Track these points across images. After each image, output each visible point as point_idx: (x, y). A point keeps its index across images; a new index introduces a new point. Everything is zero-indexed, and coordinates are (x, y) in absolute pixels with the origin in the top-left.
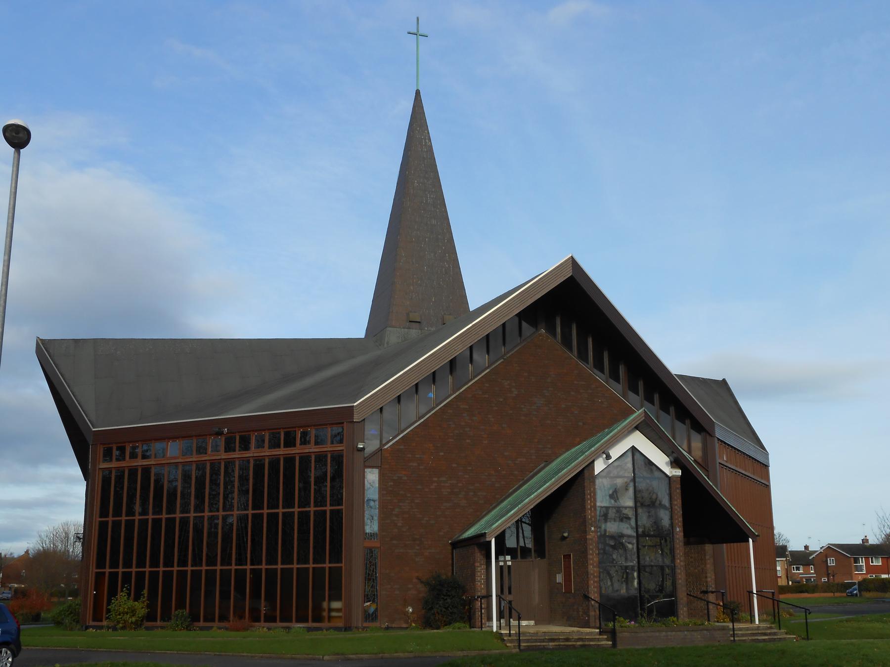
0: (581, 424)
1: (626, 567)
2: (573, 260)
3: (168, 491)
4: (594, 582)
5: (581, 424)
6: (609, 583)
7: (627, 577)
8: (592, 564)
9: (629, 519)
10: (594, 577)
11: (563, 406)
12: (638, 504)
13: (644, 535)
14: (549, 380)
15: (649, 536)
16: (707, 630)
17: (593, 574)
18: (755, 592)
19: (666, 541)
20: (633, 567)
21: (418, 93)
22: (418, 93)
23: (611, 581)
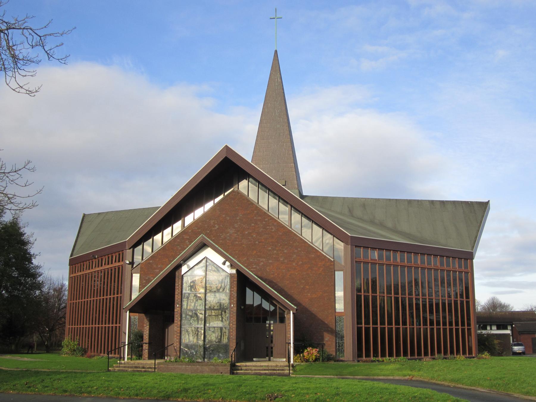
0: (257, 242)
1: (198, 328)
2: (226, 146)
3: (372, 280)
4: (177, 336)
5: (257, 242)
6: (187, 337)
7: (198, 334)
8: (177, 326)
9: (201, 299)
10: (177, 333)
11: (246, 233)
12: (208, 291)
13: (211, 309)
14: (238, 218)
15: (214, 309)
16: (213, 365)
17: (176, 332)
18: (127, 343)
19: (225, 312)
20: (201, 327)
21: (276, 52)
22: (276, 52)
23: (189, 335)
